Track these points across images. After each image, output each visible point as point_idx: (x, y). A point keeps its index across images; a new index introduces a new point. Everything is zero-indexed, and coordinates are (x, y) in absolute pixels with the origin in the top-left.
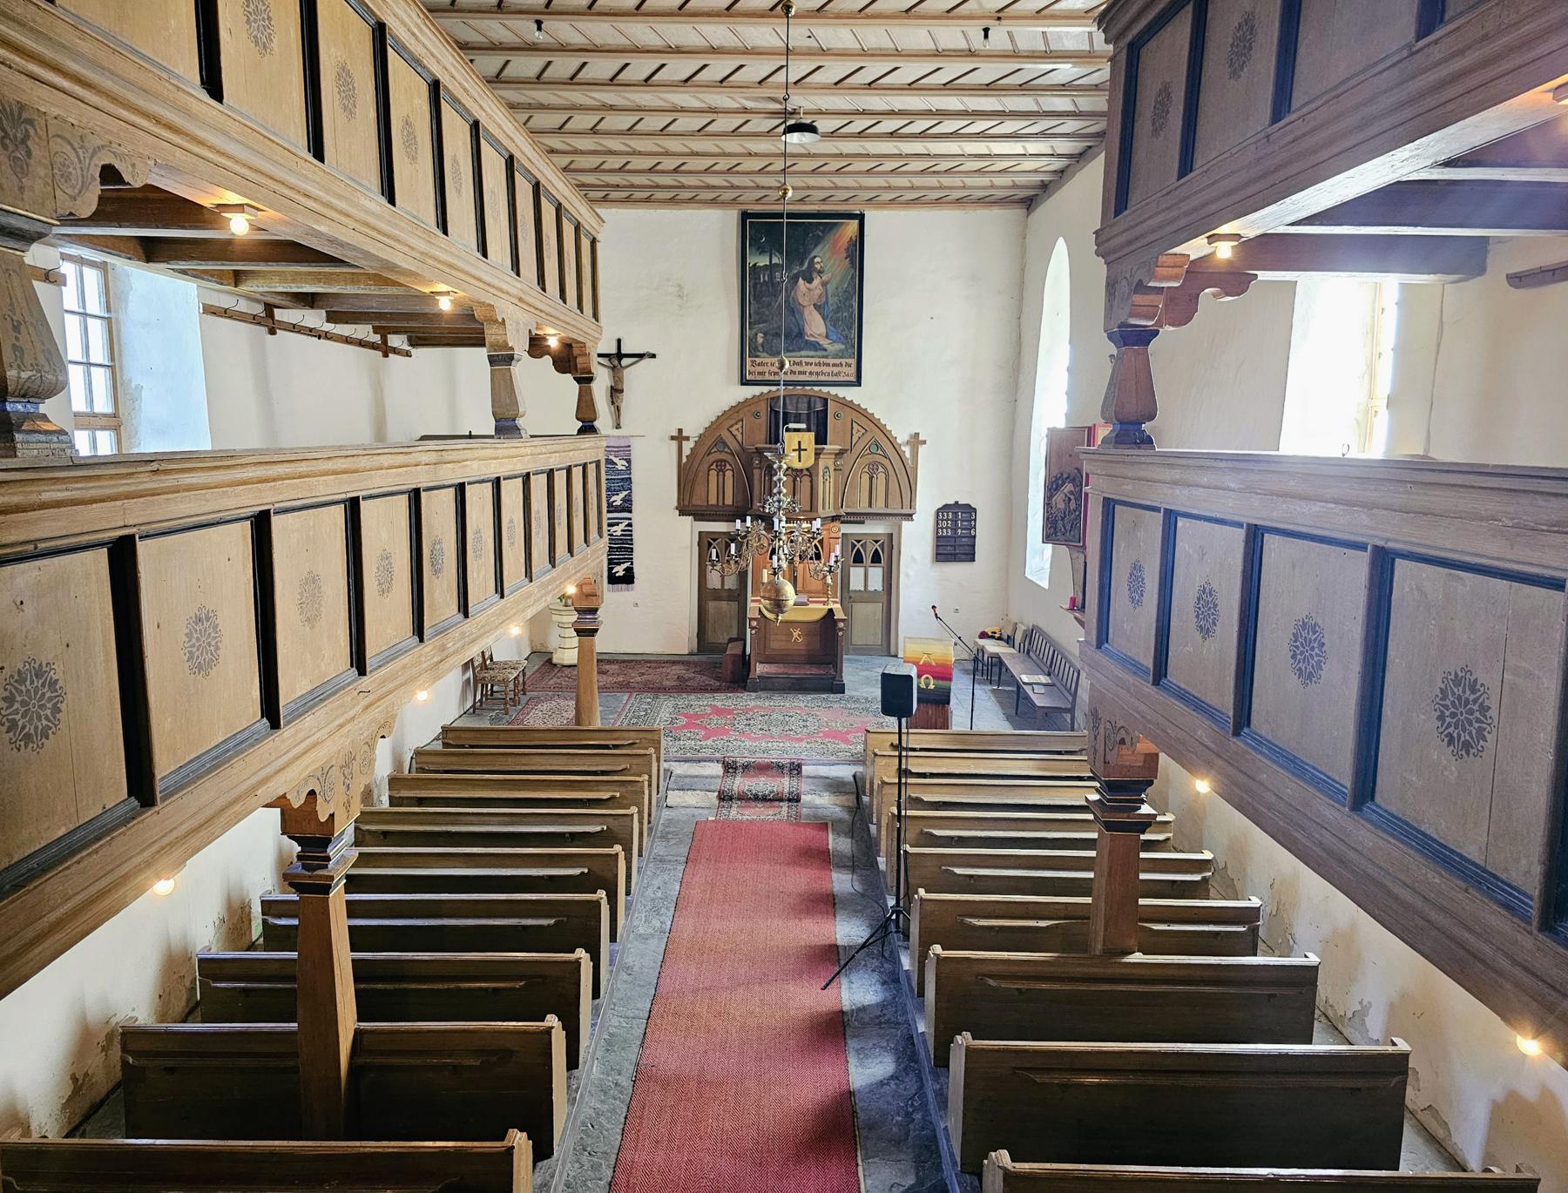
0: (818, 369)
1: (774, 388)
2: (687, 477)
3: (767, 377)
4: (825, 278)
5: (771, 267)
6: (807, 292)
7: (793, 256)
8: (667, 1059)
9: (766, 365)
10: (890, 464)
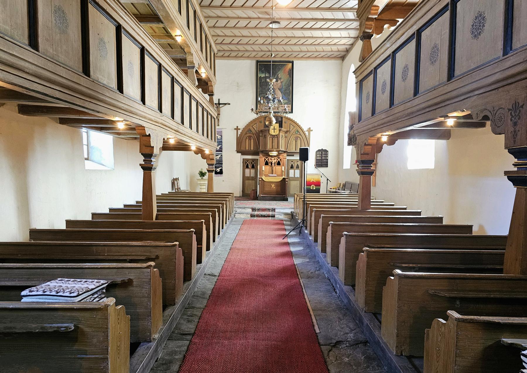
1: (266, 114)
4: (282, 80)
5: (266, 78)
7: (272, 73)
8: (238, 246)
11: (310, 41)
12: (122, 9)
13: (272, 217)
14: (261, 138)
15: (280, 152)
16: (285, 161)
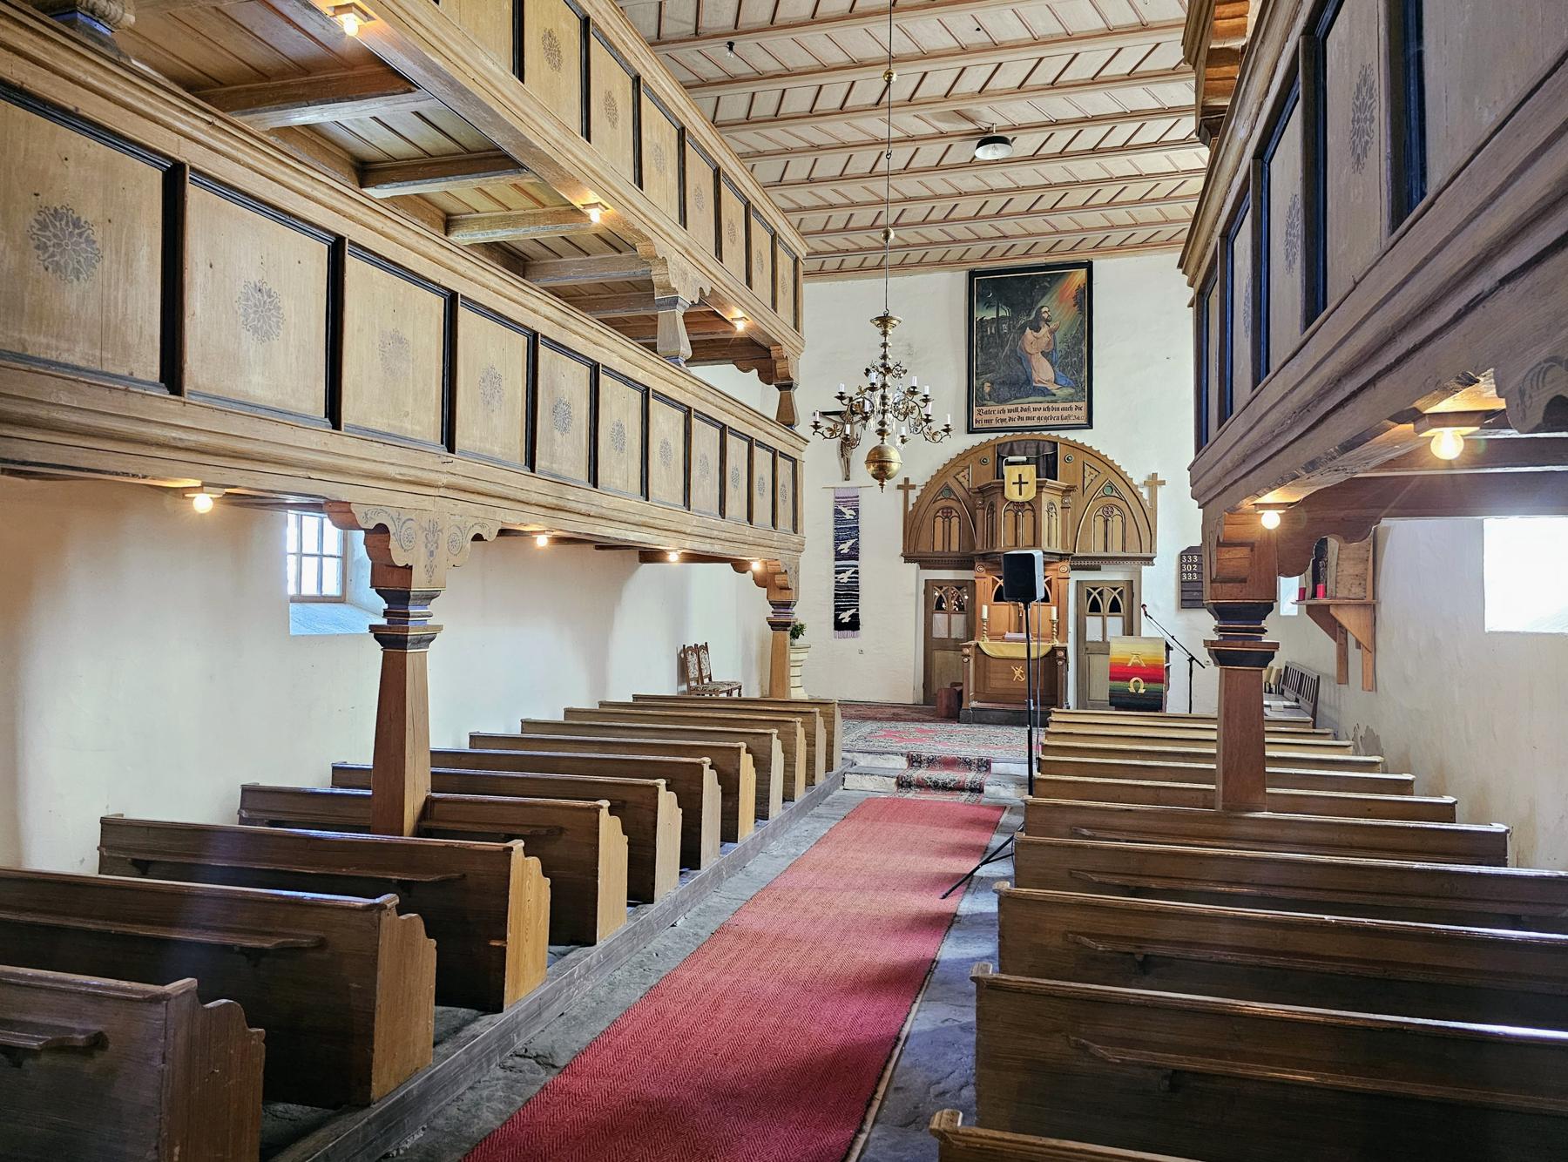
0: (1047, 414)
2: (913, 525)
3: (994, 424)
5: (998, 319)
6: (1034, 341)
7: (1022, 305)
9: (996, 413)
10: (1125, 503)
11: (1135, 191)
12: (183, 110)
13: (972, 790)
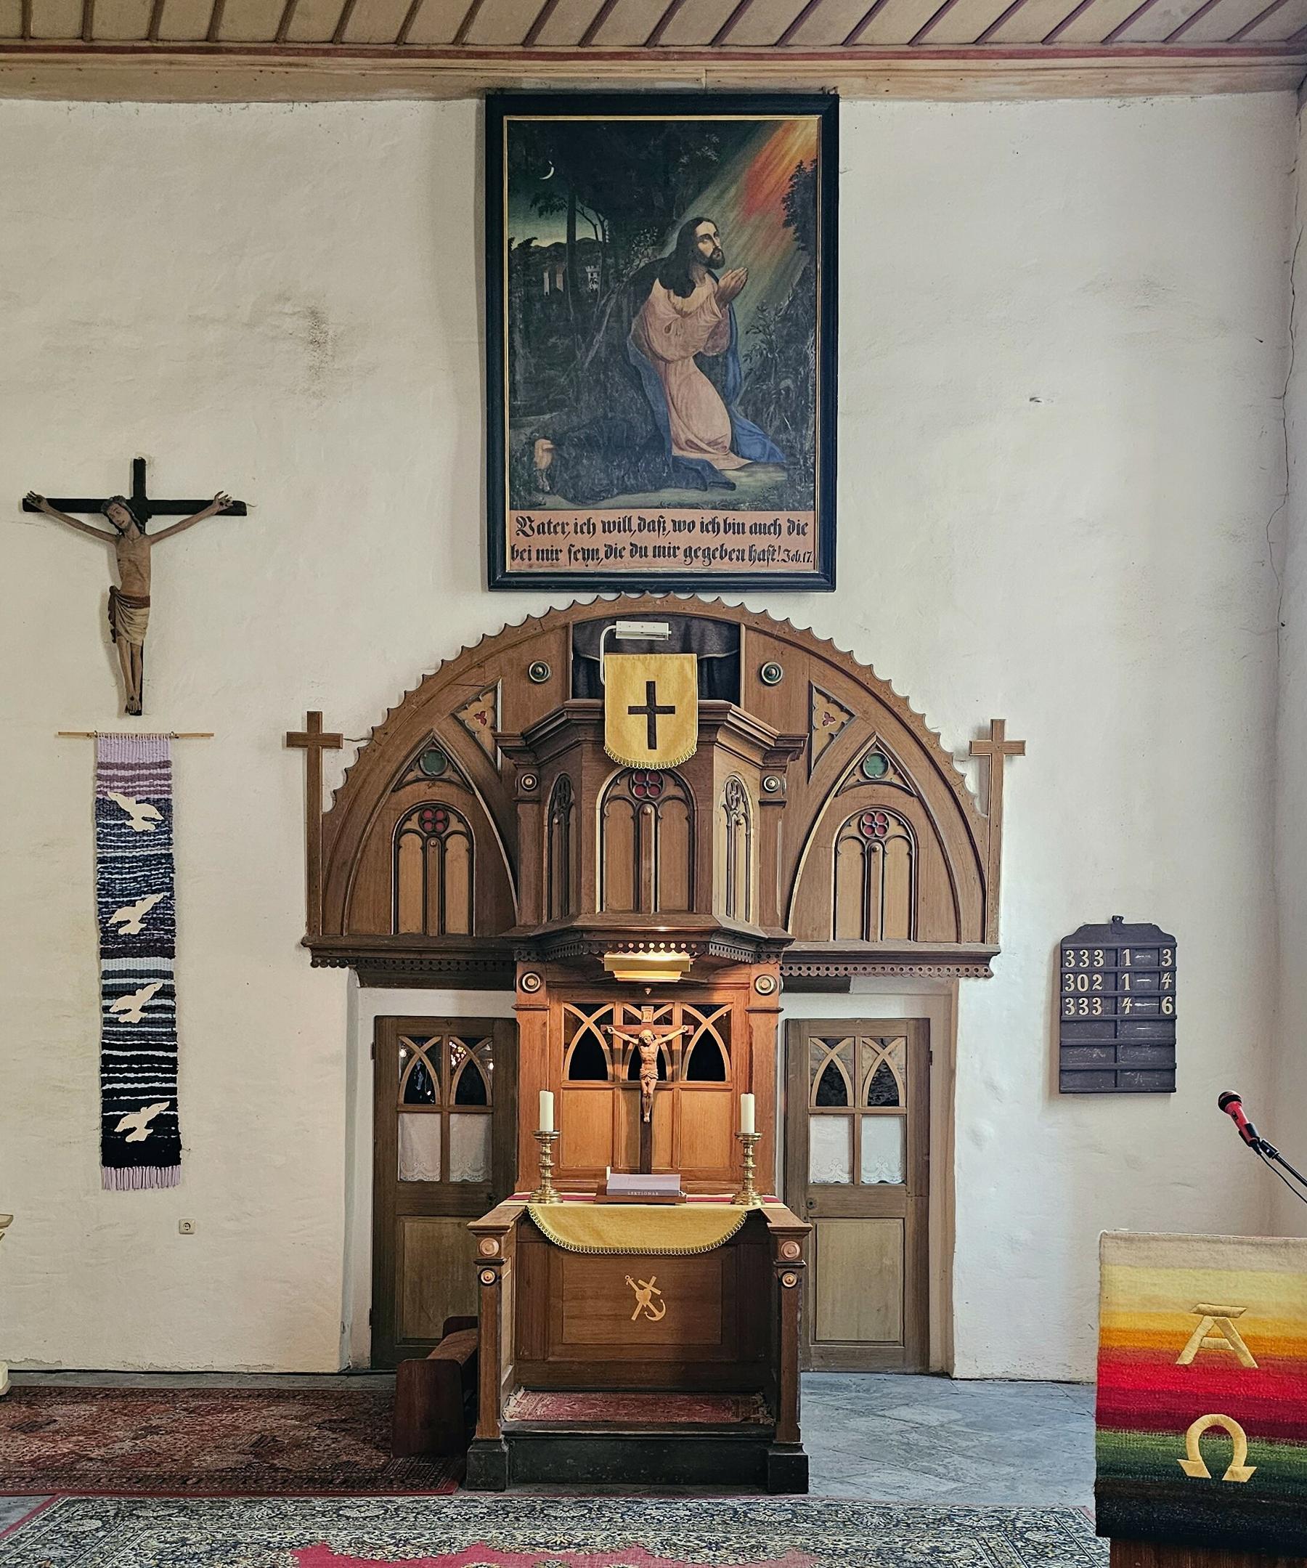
4: (726, 280)
14: (526, 813)
15: (718, 949)
16: (767, 1037)
